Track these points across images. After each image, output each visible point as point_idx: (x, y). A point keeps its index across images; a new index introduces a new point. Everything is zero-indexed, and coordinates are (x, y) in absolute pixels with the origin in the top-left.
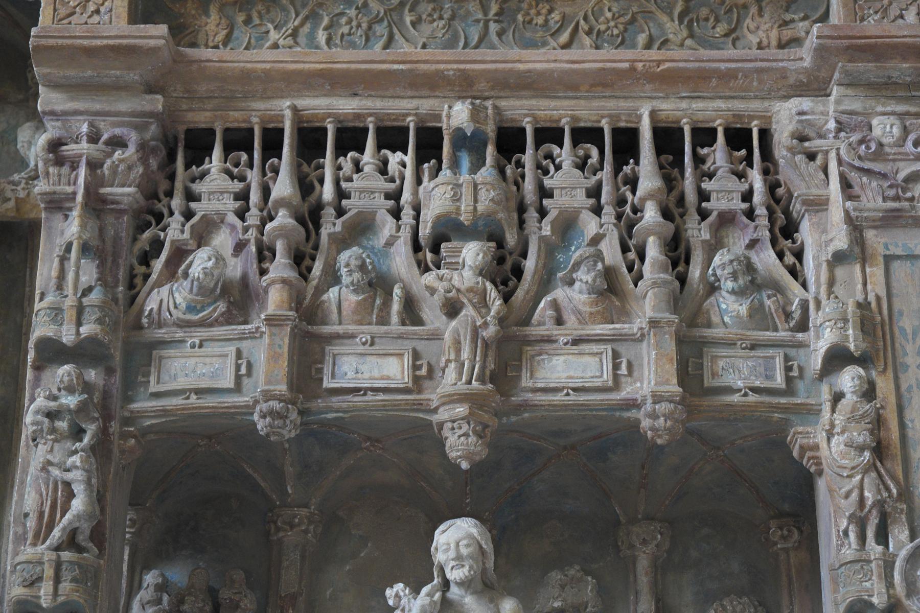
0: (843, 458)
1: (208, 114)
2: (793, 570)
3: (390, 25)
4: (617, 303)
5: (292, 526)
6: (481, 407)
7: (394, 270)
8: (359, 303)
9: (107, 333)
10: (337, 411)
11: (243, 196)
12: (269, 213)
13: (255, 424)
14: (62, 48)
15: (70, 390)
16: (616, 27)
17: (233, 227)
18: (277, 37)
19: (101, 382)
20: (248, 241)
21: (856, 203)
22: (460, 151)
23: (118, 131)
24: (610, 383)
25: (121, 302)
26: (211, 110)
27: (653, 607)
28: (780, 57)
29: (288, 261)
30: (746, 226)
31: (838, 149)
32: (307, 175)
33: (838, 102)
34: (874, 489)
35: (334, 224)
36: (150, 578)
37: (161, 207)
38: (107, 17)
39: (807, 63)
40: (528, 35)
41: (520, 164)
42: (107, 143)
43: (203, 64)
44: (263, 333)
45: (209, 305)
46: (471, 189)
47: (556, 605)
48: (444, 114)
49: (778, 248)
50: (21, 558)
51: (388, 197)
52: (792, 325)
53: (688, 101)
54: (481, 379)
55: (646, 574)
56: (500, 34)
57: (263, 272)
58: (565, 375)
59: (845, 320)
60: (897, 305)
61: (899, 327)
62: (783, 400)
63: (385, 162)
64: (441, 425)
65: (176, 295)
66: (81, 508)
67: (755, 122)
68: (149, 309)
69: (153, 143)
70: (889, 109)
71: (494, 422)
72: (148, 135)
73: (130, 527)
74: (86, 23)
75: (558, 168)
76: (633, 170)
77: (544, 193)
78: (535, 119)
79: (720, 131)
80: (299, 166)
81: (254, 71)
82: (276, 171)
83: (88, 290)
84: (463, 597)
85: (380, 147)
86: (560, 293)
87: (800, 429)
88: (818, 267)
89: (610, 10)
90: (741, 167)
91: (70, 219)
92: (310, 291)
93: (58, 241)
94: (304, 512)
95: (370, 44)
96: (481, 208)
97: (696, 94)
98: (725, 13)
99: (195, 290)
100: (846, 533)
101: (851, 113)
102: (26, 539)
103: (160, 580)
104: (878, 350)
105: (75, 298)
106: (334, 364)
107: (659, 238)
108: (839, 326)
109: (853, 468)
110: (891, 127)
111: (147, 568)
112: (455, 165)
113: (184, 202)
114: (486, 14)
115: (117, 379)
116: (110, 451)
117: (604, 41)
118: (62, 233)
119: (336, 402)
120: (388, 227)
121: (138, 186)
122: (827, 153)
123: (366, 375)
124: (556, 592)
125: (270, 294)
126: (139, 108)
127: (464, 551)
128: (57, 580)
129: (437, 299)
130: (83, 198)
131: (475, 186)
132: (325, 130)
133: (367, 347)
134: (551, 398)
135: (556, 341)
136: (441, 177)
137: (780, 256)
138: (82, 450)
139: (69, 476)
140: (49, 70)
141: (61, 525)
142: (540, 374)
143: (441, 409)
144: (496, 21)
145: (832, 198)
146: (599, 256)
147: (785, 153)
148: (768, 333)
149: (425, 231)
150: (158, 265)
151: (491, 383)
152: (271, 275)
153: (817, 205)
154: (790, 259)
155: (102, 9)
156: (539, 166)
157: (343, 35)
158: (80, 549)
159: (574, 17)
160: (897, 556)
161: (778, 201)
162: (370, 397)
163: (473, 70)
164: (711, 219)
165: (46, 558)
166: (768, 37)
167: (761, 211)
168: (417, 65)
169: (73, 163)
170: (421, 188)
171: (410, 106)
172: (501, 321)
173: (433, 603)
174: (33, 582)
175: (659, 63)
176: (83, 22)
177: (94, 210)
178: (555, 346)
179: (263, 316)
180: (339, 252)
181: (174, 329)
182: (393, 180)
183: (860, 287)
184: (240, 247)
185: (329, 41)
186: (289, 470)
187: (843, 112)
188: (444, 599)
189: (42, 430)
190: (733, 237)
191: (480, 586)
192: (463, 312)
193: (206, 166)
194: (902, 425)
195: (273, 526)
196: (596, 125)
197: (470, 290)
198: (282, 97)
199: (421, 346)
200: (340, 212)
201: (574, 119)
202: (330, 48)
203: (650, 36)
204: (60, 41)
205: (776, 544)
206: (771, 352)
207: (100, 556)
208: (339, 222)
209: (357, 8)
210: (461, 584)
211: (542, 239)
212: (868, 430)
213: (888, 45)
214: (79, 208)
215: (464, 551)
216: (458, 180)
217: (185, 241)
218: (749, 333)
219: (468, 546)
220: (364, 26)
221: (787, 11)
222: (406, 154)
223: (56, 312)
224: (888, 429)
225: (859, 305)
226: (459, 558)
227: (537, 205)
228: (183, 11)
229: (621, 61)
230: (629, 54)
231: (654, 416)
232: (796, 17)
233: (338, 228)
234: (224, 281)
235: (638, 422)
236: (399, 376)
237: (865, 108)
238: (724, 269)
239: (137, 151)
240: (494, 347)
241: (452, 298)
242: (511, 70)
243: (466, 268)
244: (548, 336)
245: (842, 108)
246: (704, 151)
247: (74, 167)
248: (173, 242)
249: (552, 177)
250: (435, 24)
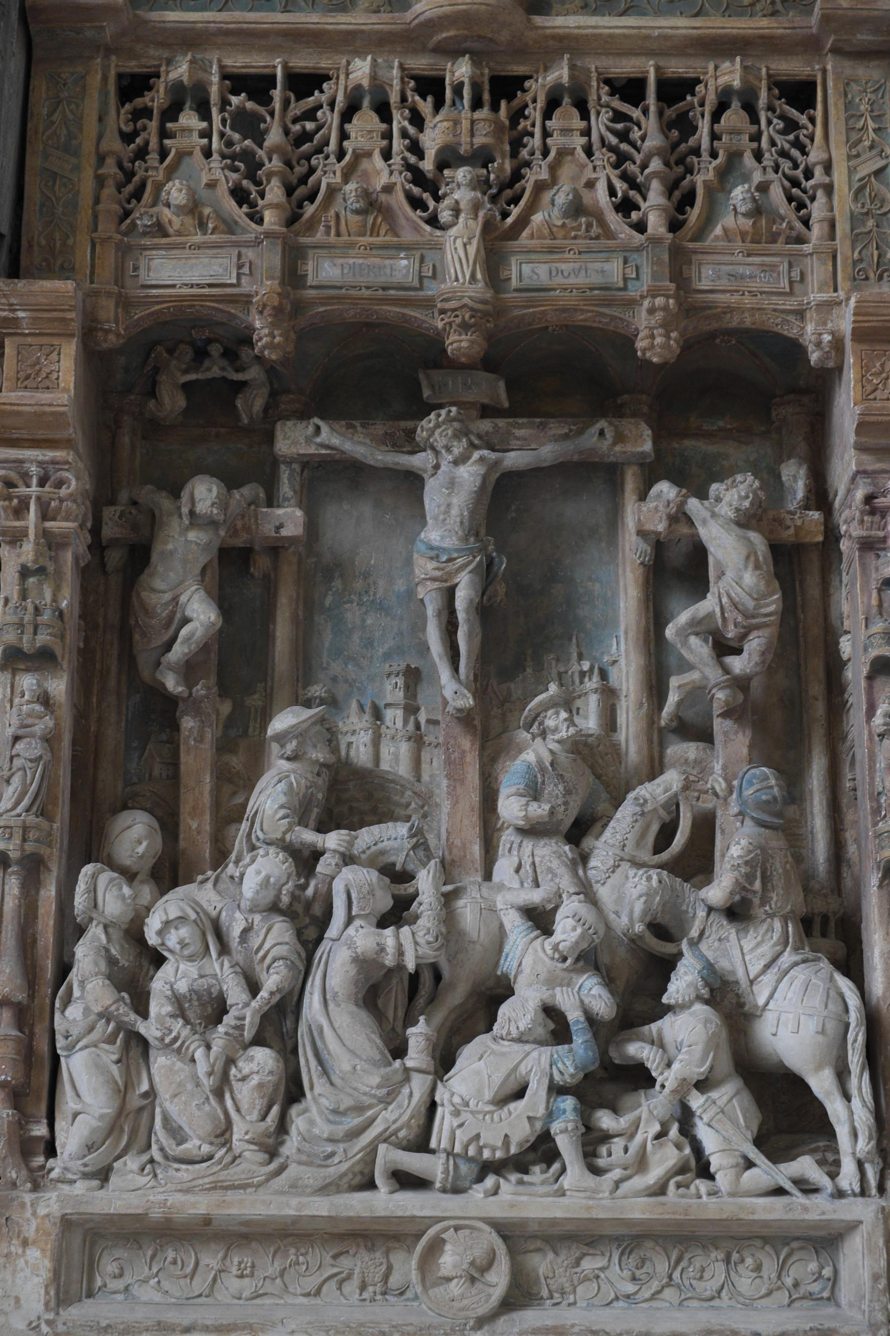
204: (880, 418)
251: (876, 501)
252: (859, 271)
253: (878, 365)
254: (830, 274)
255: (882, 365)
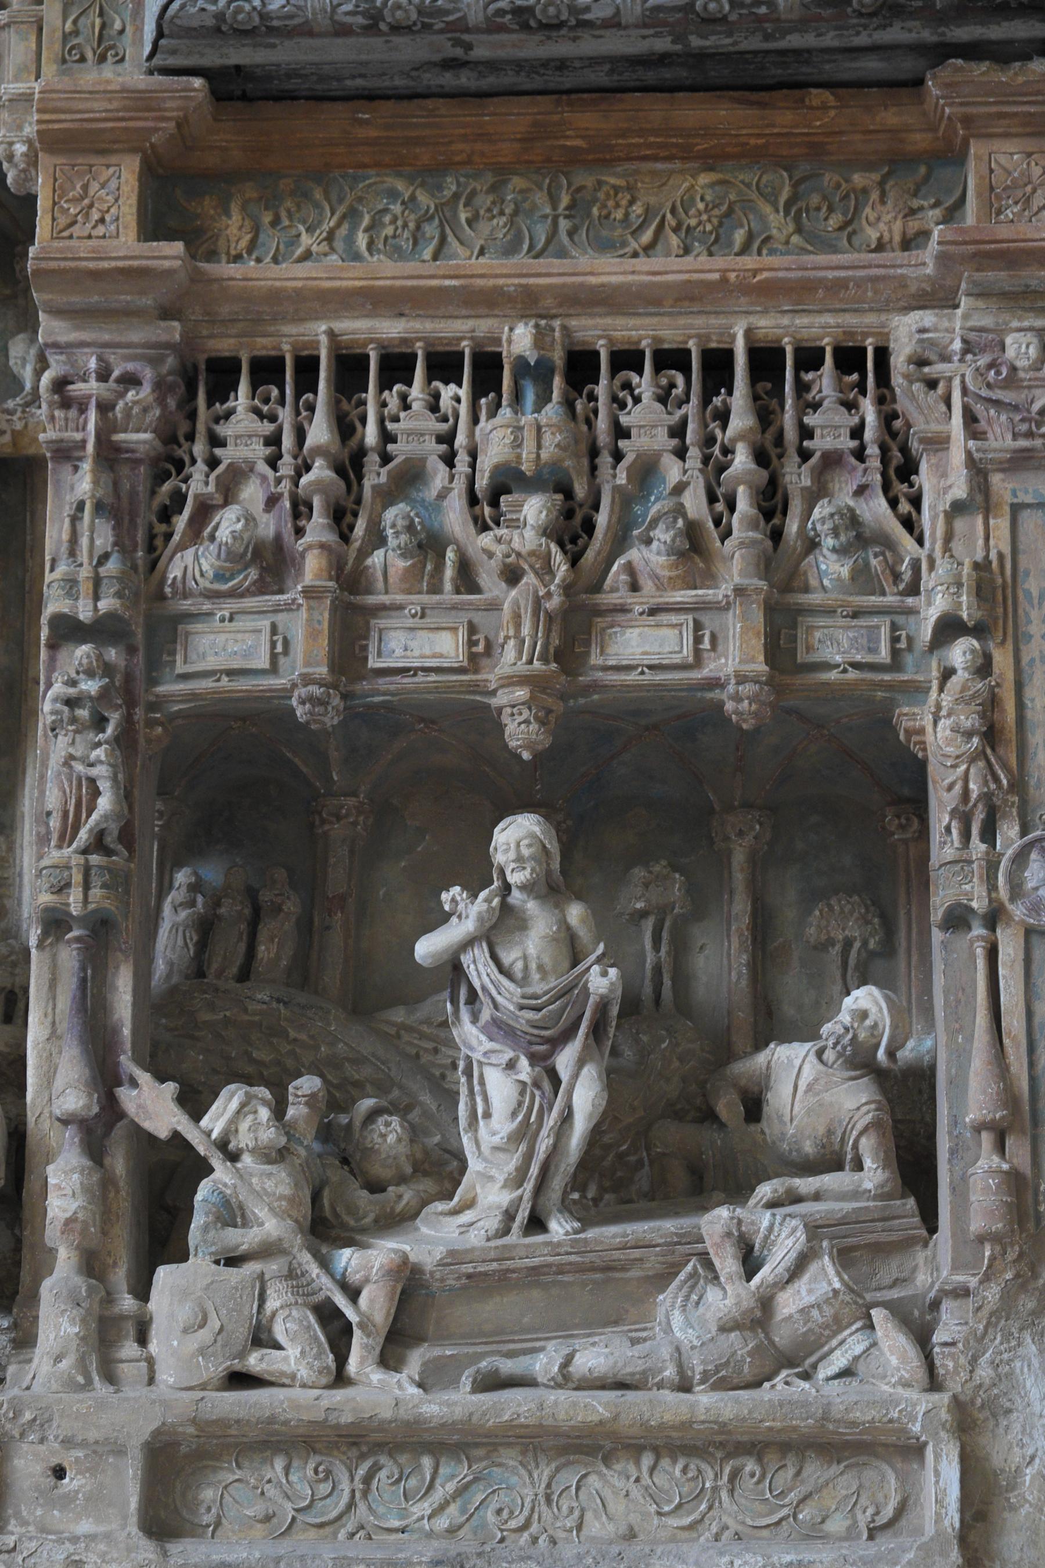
0: (948, 745)
1: (232, 341)
2: (912, 864)
3: (441, 225)
4: (701, 565)
5: (339, 818)
6: (543, 691)
7: (447, 528)
8: (407, 570)
9: (128, 608)
10: (384, 694)
11: (274, 441)
12: (305, 461)
13: (293, 710)
14: (63, 272)
15: (90, 674)
16: (709, 221)
17: (264, 478)
18: (310, 242)
19: (122, 663)
20: (281, 495)
21: (979, 443)
22: (523, 378)
23: (130, 367)
24: (691, 659)
25: (141, 569)
26: (237, 336)
27: (749, 908)
28: (899, 262)
29: (326, 521)
30: (854, 469)
31: (963, 376)
32: (347, 414)
33: (966, 317)
34: (980, 780)
35: (379, 474)
36: (182, 877)
37: (181, 453)
38: (113, 227)
39: (929, 270)
40: (605, 233)
41: (592, 398)
42: (119, 381)
43: (224, 283)
44: (300, 605)
45: (239, 572)
46: (534, 432)
47: (638, 906)
48: (504, 337)
49: (891, 494)
50: (46, 862)
51: (440, 439)
52: (902, 587)
53: (790, 315)
54: (544, 659)
55: (742, 870)
56: (571, 234)
57: (299, 532)
58: (640, 650)
59: (959, 585)
60: (1023, 562)
61: (1024, 590)
62: (887, 677)
63: (437, 396)
64: (500, 710)
65: (202, 561)
66: (108, 807)
67: (870, 340)
68: (172, 576)
69: (170, 378)
70: (1026, 324)
71: (559, 707)
72: (165, 369)
73: (159, 819)
74: (90, 237)
75: (637, 400)
76: (724, 402)
77: (621, 432)
78: (611, 340)
79: (829, 350)
80: (338, 402)
81: (284, 290)
82: (311, 408)
83: (104, 558)
84: (525, 902)
85: (429, 379)
86: (634, 554)
87: (906, 710)
88: (934, 519)
89: (702, 199)
90: (852, 396)
91: (80, 472)
92: (352, 554)
93: (68, 497)
94: (351, 801)
95: (419, 248)
96: (545, 455)
97: (800, 307)
98: (842, 199)
99: (223, 555)
100: (948, 829)
101: (981, 330)
102: (49, 840)
103: (193, 879)
104: (996, 620)
105: (90, 568)
106: (380, 640)
107: (750, 488)
108: (951, 591)
109: (958, 757)
110: (1027, 347)
111: (178, 864)
112: (518, 398)
113: (208, 447)
114: (555, 208)
115: (140, 658)
116: (135, 742)
117: (694, 239)
118: (72, 488)
119: (383, 683)
120: (439, 477)
121: (154, 431)
122: (950, 379)
123: (416, 653)
124: (639, 890)
125: (307, 561)
126: (154, 339)
127: (526, 852)
128: (87, 886)
129: (494, 564)
130: (95, 447)
131: (539, 428)
132: (367, 357)
133: (417, 620)
134: (623, 677)
135: (630, 611)
136: (498, 420)
137: (893, 503)
138: (107, 742)
139: (94, 772)
140: (50, 296)
141: (88, 826)
142: (612, 649)
143: (500, 692)
144: (566, 217)
145: (953, 434)
146: (680, 510)
147: (901, 381)
148: (873, 598)
149: (482, 483)
150: (181, 522)
151: (556, 661)
152: (308, 539)
153: (936, 443)
154: (905, 507)
155: (108, 218)
156: (615, 399)
157: (386, 238)
158: (108, 852)
159: (660, 209)
160: (1003, 855)
161: (893, 435)
162: (421, 678)
163: (538, 285)
164: (813, 461)
165: (73, 863)
166: (890, 231)
167: (873, 450)
168: (472, 281)
169: (81, 404)
170: (478, 429)
171: (465, 328)
172: (567, 589)
173: (491, 909)
174: (61, 889)
175: (755, 272)
176: (86, 234)
177: (107, 459)
178: (629, 616)
179: (299, 588)
180: (385, 508)
181: (201, 600)
182: (445, 419)
183: (981, 542)
184: (272, 501)
185: (370, 246)
186: (334, 755)
187: (972, 329)
188: (504, 906)
189: (62, 720)
190: (840, 482)
191: (544, 889)
192: (524, 580)
193: (230, 404)
194: (1020, 705)
195: (317, 818)
196: (681, 346)
197: (532, 553)
198: (317, 319)
199: (478, 618)
200: (386, 459)
201: (656, 339)
202: (371, 255)
203: (750, 230)
204: (63, 264)
205: (893, 834)
206: (875, 620)
207: (130, 860)
208: (384, 471)
209: (403, 203)
210: (523, 888)
211: (616, 489)
212: (978, 713)
213: (1023, 251)
214: (90, 460)
215: (526, 852)
216: (518, 421)
217: (210, 496)
218: (851, 599)
219: (529, 846)
220: (412, 225)
221: (915, 195)
222: (460, 385)
223: (71, 584)
224: (1003, 711)
225: (976, 566)
226: (520, 859)
227: (612, 447)
228: (199, 211)
229: (710, 271)
230: (720, 262)
231: (737, 698)
232: (925, 204)
233: (383, 479)
234: (256, 545)
235: (721, 704)
236: (453, 654)
237: (997, 324)
238: (823, 524)
239: (153, 391)
240: (559, 621)
241: (511, 564)
242: (582, 285)
243: (528, 527)
244: (621, 605)
245: (970, 324)
246: (809, 376)
247: (83, 410)
248: (196, 496)
249: (629, 413)
250: (495, 221)
251: (71, 387)
252: (72, 48)
253: (78, 187)
254: (32, 56)
255: (85, 187)
